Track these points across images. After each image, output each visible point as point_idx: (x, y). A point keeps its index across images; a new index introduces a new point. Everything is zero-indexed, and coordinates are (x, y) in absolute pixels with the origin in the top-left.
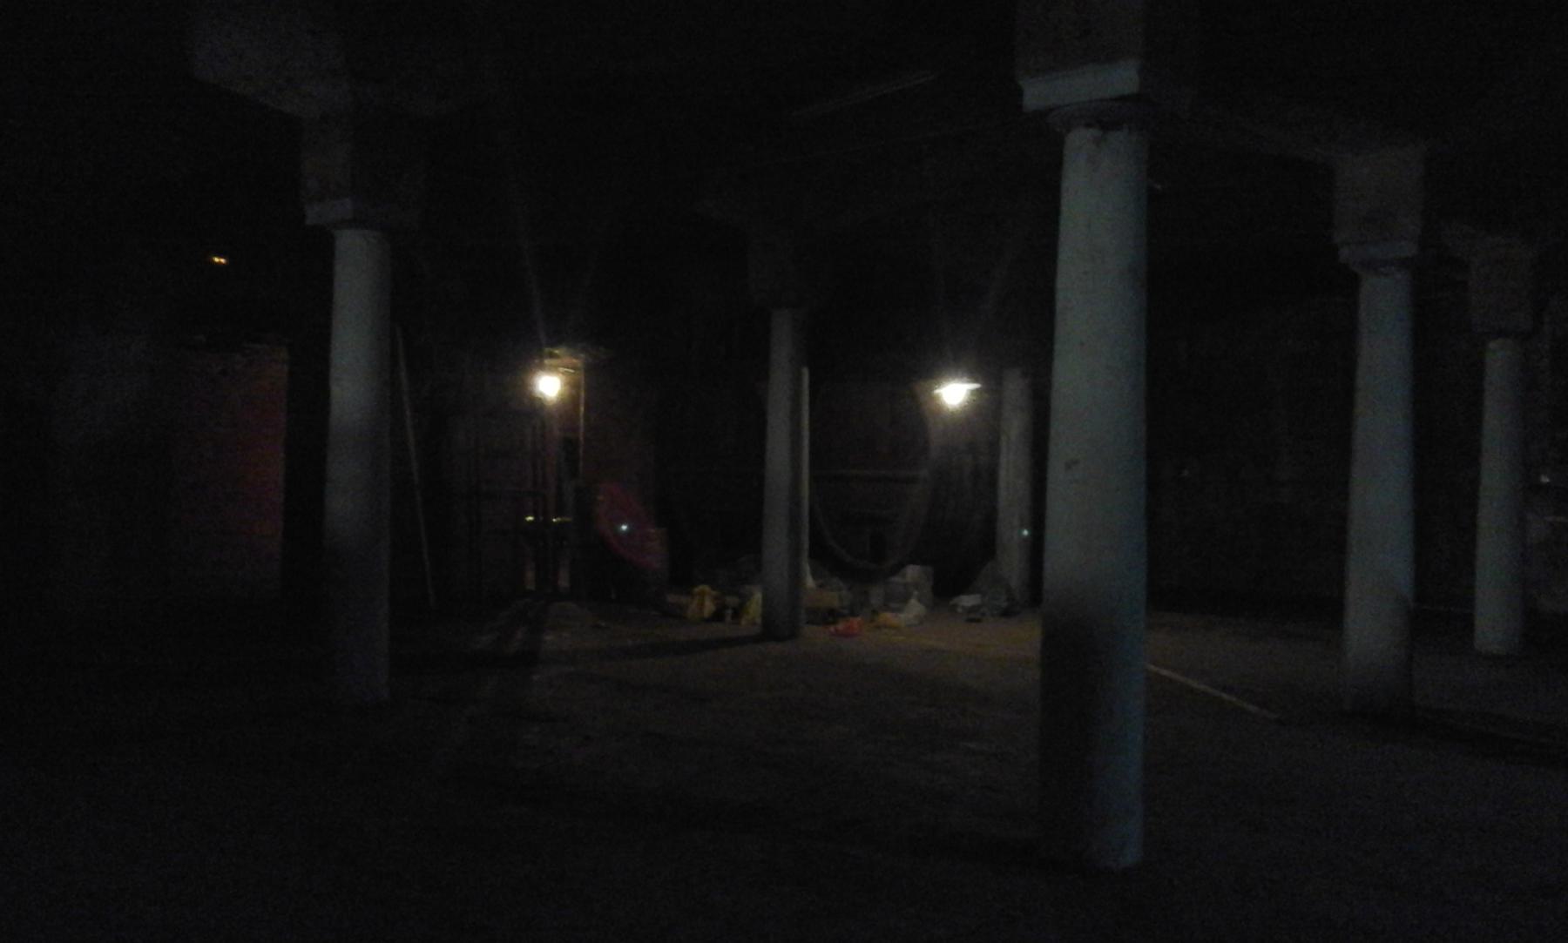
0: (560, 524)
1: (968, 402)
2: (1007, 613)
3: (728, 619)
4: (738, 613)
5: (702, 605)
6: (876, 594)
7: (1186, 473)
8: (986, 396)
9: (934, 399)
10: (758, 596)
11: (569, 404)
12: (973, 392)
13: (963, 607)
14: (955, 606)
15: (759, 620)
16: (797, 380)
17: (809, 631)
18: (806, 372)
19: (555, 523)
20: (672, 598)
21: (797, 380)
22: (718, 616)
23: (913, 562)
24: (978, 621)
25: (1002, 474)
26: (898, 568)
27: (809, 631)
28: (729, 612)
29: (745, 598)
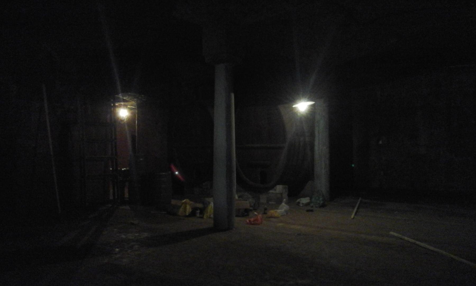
0: (124, 170)
1: (306, 113)
2: (323, 206)
3: (198, 215)
4: (202, 211)
5: (185, 208)
6: (263, 198)
7: (381, 142)
8: (305, 114)
9: (292, 110)
10: (212, 205)
11: (131, 122)
12: (313, 106)
13: (303, 203)
14: (299, 203)
15: (212, 216)
16: (229, 98)
17: (238, 221)
18: (233, 96)
19: (123, 170)
20: (173, 202)
21: (229, 98)
22: (193, 214)
23: (279, 184)
24: (312, 211)
25: (316, 143)
26: (273, 187)
27: (238, 221)
28: (198, 211)
29: (206, 205)
